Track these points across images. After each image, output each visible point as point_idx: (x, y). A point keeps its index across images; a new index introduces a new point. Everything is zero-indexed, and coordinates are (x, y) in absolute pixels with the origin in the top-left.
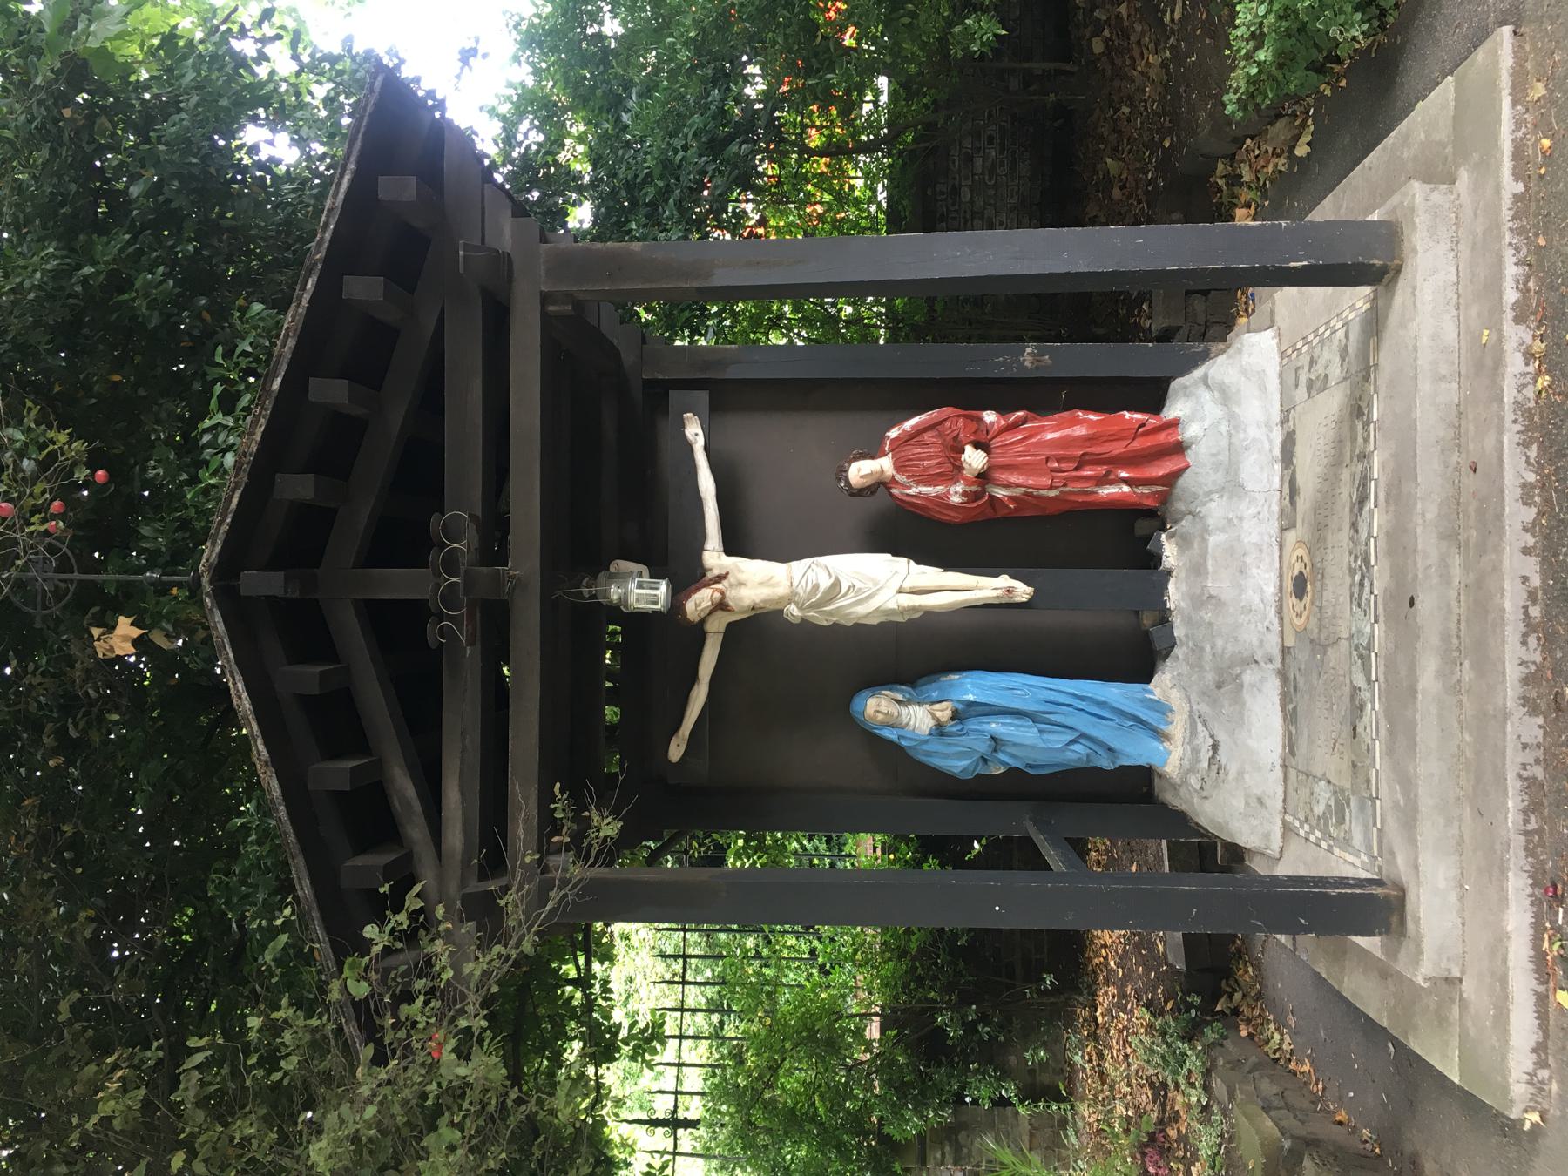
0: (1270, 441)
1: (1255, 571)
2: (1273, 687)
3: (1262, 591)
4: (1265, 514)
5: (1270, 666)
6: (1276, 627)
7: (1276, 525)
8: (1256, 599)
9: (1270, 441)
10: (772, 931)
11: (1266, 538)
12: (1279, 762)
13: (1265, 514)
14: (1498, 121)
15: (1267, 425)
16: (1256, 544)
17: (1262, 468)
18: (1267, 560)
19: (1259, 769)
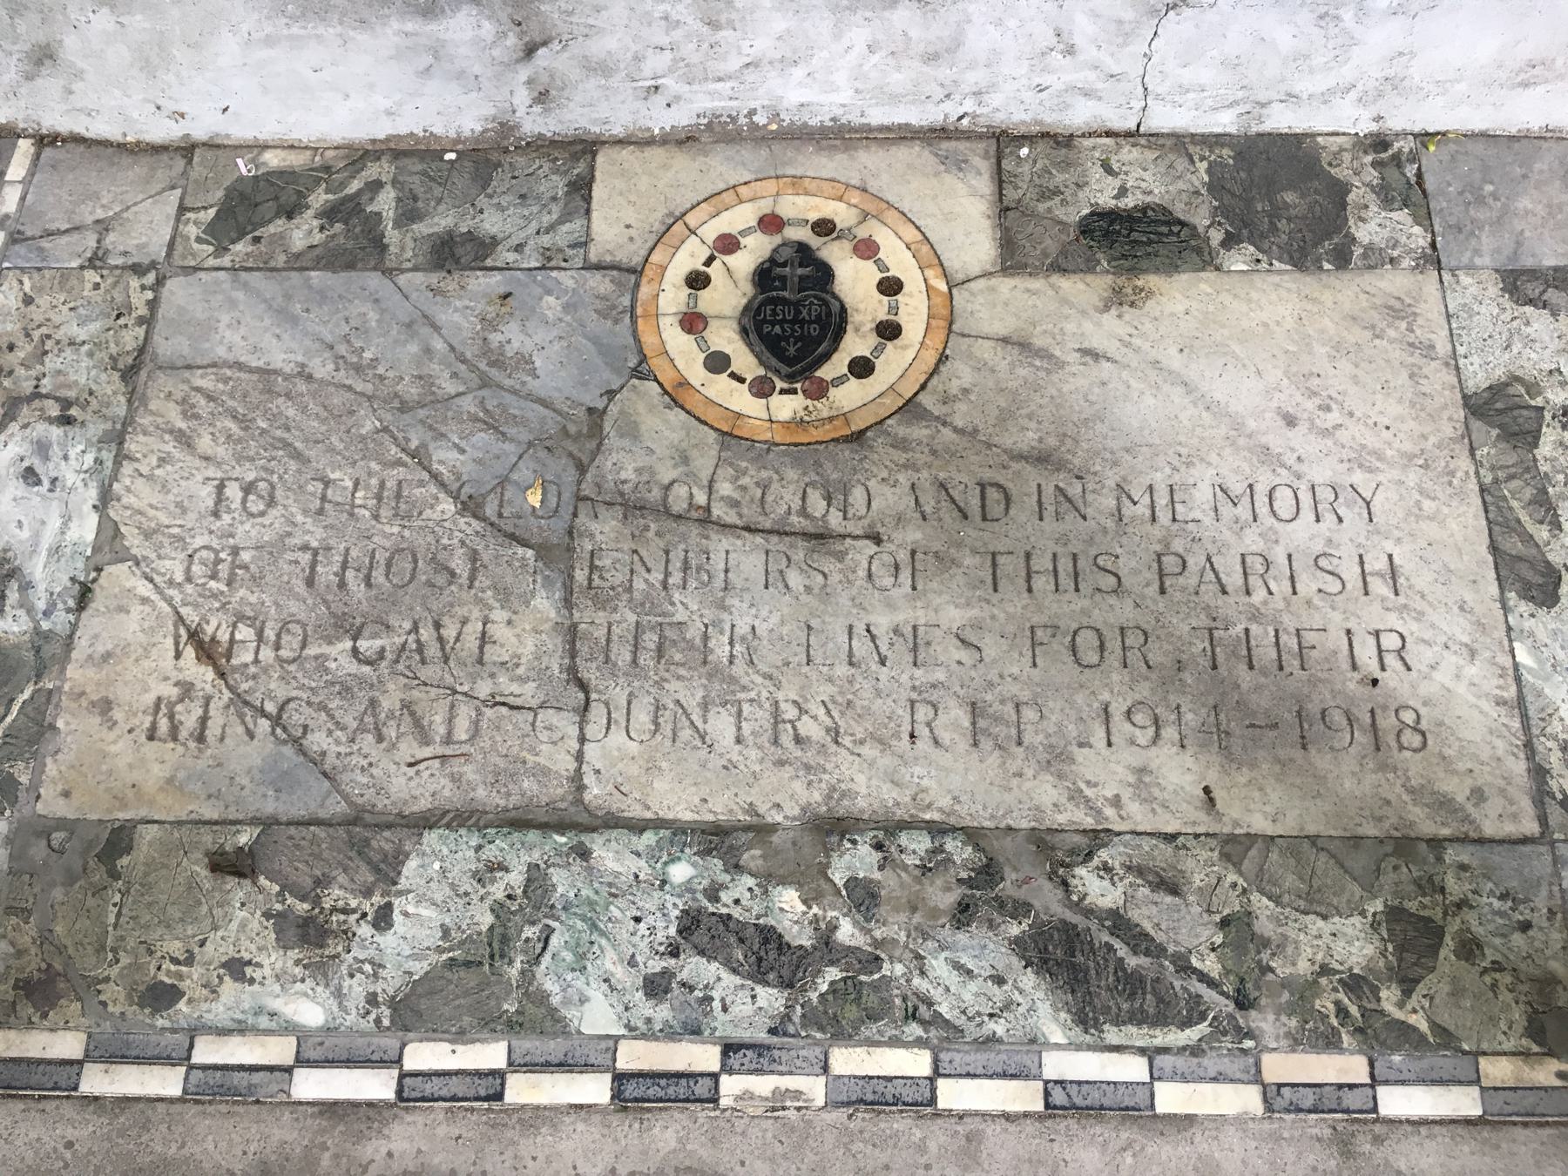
0: (1326, 98)
1: (859, 35)
2: (453, 113)
3: (786, 63)
4: (1063, 73)
5: (522, 97)
6: (661, 119)
7: (1013, 105)
8: (762, 45)
9: (1326, 98)
10: (400, 505)
11: (973, 78)
12: (199, 133)
13: (1063, 73)
14: (461, 1037)
15: (1393, 83)
16: (955, 45)
17: (1232, 65)
18: (898, 80)
19: (148, 68)
